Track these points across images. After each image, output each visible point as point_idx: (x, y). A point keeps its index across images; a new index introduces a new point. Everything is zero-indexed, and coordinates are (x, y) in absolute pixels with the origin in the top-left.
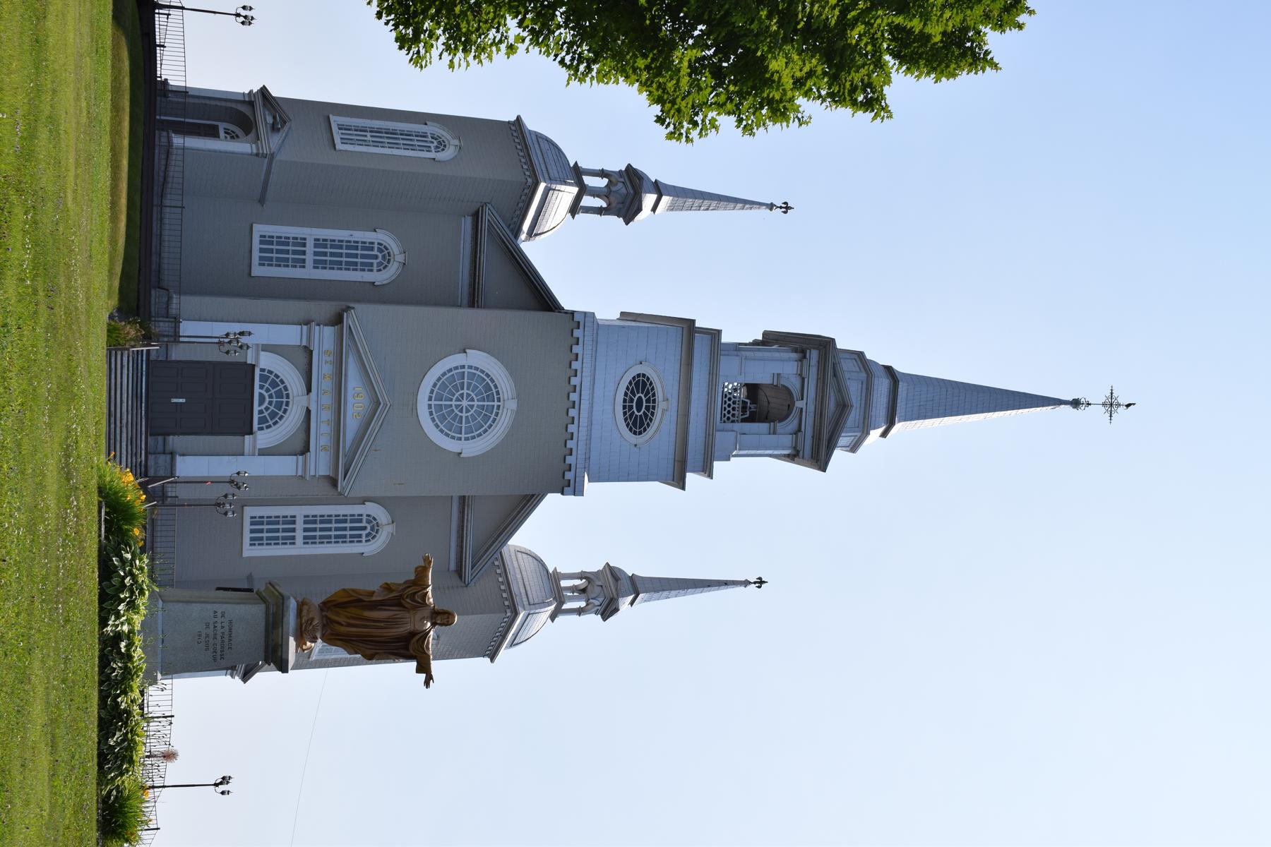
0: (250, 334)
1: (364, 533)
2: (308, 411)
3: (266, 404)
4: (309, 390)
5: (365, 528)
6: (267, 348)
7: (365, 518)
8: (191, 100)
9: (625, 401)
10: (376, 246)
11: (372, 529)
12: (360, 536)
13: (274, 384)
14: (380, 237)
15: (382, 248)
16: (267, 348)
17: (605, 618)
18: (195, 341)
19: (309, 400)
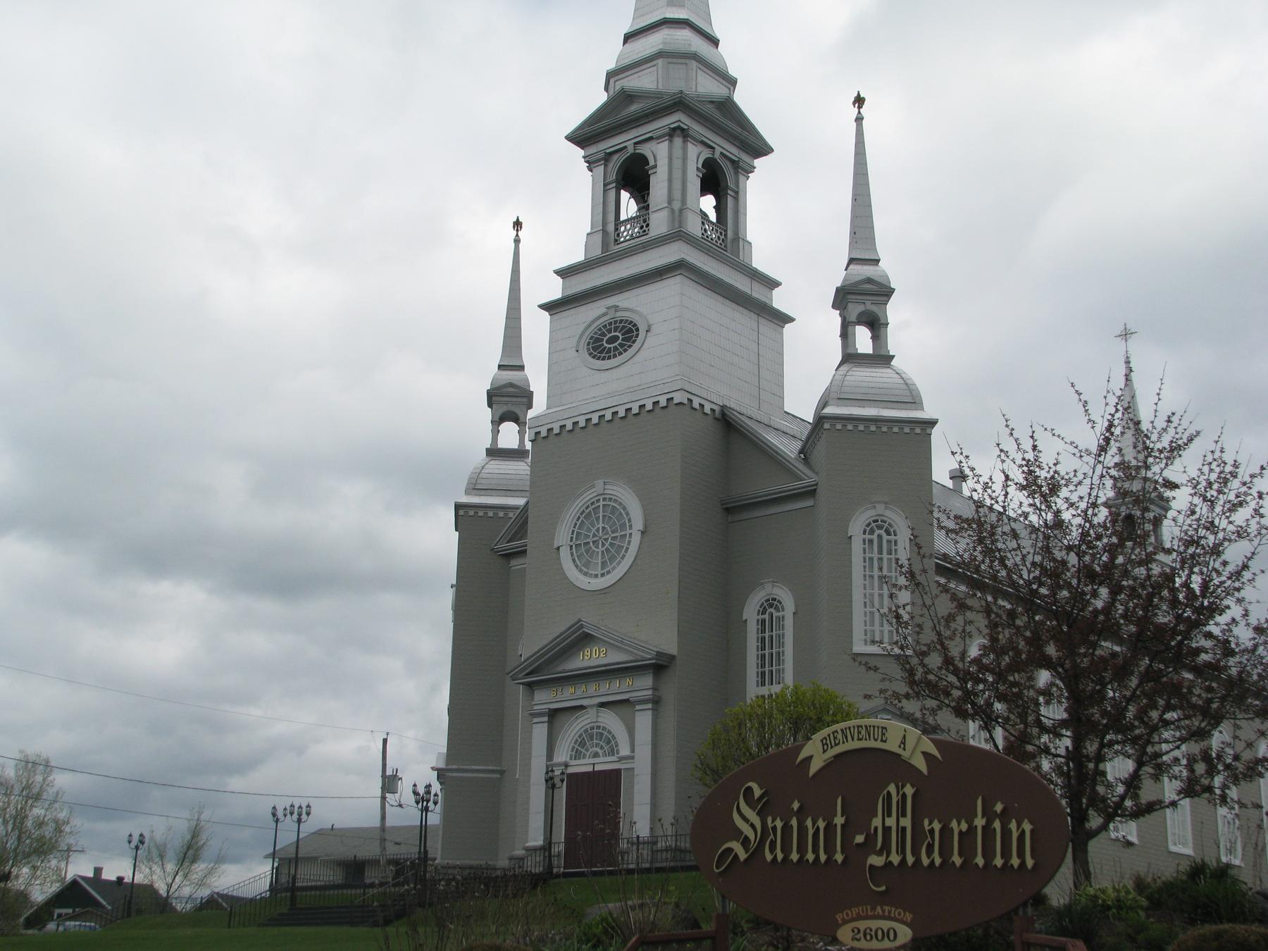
1: (885, 537)
2: (602, 705)
3: (598, 750)
4: (582, 707)
5: (880, 537)
6: (550, 755)
7: (867, 537)
9: (620, 354)
11: (880, 527)
14: (856, 528)
16: (550, 755)
17: (762, 149)
19: (592, 706)
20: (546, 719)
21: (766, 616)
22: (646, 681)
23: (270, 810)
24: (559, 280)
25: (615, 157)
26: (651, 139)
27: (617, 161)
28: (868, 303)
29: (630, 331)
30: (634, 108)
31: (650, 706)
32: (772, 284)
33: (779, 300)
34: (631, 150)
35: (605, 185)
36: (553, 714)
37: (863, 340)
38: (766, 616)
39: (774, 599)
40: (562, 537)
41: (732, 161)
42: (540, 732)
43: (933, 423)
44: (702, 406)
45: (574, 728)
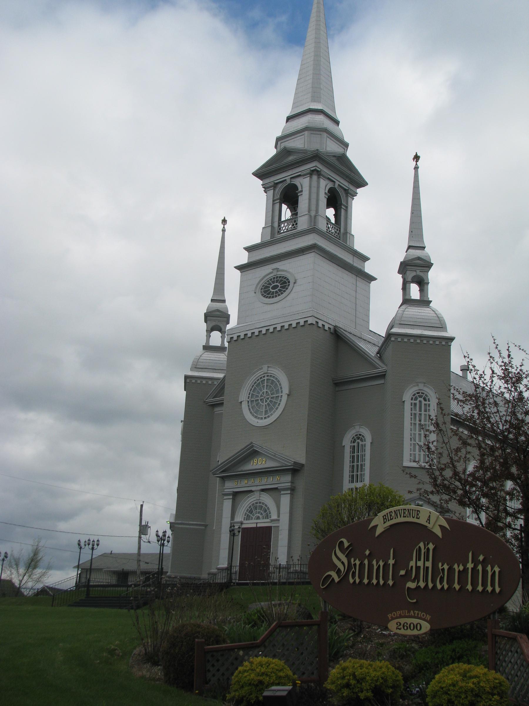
0: (157, 531)
2: (263, 490)
4: (251, 491)
8: (237, 562)
10: (413, 401)
11: (420, 397)
12: (425, 405)
13: (251, 512)
15: (414, 397)
16: (233, 517)
18: (290, 556)
19: (256, 491)
20: (231, 497)
21: (356, 444)
22: (288, 478)
23: (77, 542)
24: (246, 253)
25: (280, 185)
26: (300, 176)
27: (280, 188)
28: (418, 272)
29: (285, 282)
30: (291, 158)
31: (289, 492)
32: (365, 259)
33: (369, 268)
34: (288, 182)
35: (273, 201)
36: (235, 495)
37: (414, 291)
38: (356, 444)
39: (360, 435)
40: (244, 396)
41: (345, 190)
42: (227, 504)
43: (452, 339)
44: (323, 325)
45: (246, 503)
